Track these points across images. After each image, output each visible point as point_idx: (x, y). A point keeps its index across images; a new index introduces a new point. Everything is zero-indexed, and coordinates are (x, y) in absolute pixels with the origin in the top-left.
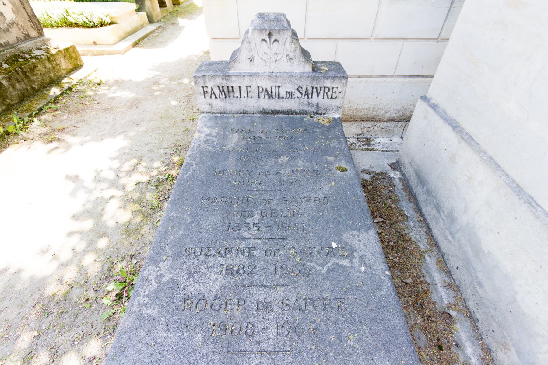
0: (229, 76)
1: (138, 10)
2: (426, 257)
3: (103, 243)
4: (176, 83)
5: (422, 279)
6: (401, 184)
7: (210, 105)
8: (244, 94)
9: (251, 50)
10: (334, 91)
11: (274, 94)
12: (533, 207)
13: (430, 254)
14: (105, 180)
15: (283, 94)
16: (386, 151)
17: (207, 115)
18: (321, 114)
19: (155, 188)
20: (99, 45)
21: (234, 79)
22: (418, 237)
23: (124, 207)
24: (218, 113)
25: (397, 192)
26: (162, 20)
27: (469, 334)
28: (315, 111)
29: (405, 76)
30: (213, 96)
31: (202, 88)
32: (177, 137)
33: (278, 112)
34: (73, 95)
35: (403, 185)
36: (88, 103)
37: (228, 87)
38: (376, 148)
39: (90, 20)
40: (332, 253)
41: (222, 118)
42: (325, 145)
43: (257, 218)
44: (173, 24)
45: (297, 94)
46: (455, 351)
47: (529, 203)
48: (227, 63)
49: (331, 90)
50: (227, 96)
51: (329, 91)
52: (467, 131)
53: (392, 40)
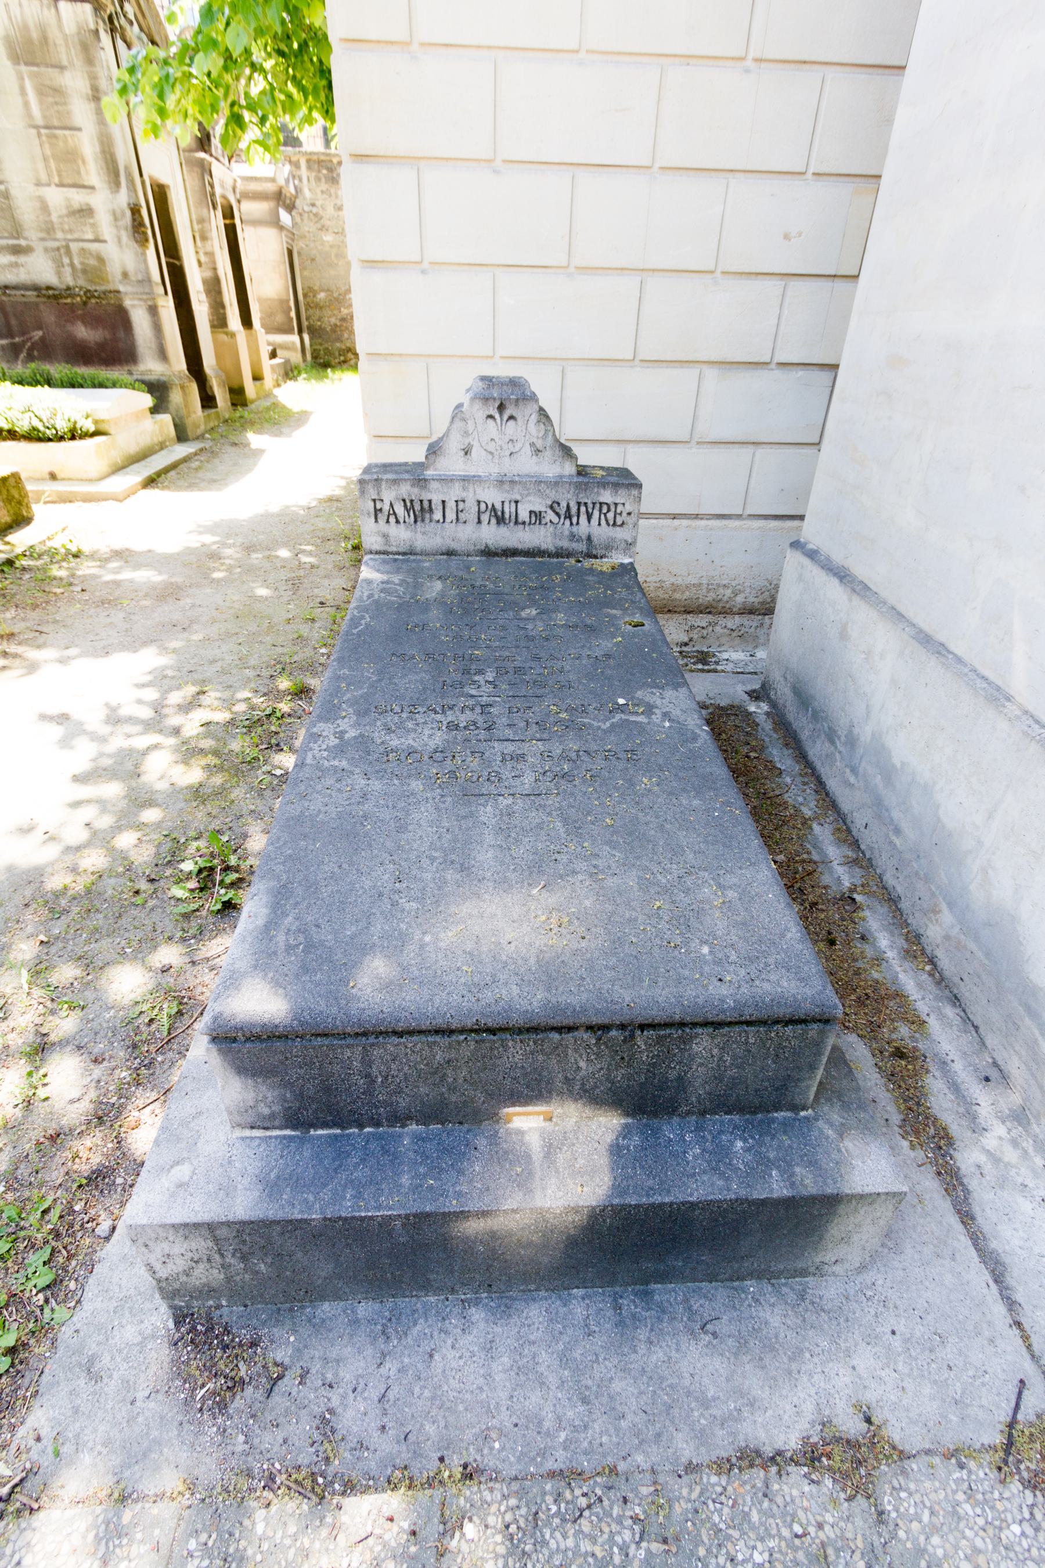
0: (426, 480)
1: (155, 410)
2: (815, 826)
3: (151, 815)
4: (260, 556)
5: (805, 856)
6: (770, 721)
7: (385, 536)
8: (451, 515)
9: (466, 433)
10: (618, 511)
11: (507, 516)
12: (944, 655)
13: (822, 821)
14: (131, 720)
15: (524, 515)
16: (742, 673)
17: (377, 556)
18: (596, 557)
19: (245, 730)
20: (63, 479)
21: (434, 485)
22: (800, 799)
23: (186, 762)
24: (399, 554)
25: (761, 734)
26: (207, 436)
27: (885, 923)
28: (585, 550)
29: (766, 517)
30: (392, 519)
31: (372, 504)
32: (280, 650)
33: (513, 552)
34: (18, 575)
35: (774, 723)
36: (58, 591)
37: (421, 501)
38: (719, 668)
39: (47, 424)
40: (621, 709)
41: (408, 561)
42: (605, 596)
43: (490, 676)
44: (236, 444)
45: (551, 516)
46: (859, 945)
47: (939, 653)
48: (421, 465)
49: (613, 508)
50: (419, 519)
51: (609, 510)
52: (860, 578)
53: (731, 446)
